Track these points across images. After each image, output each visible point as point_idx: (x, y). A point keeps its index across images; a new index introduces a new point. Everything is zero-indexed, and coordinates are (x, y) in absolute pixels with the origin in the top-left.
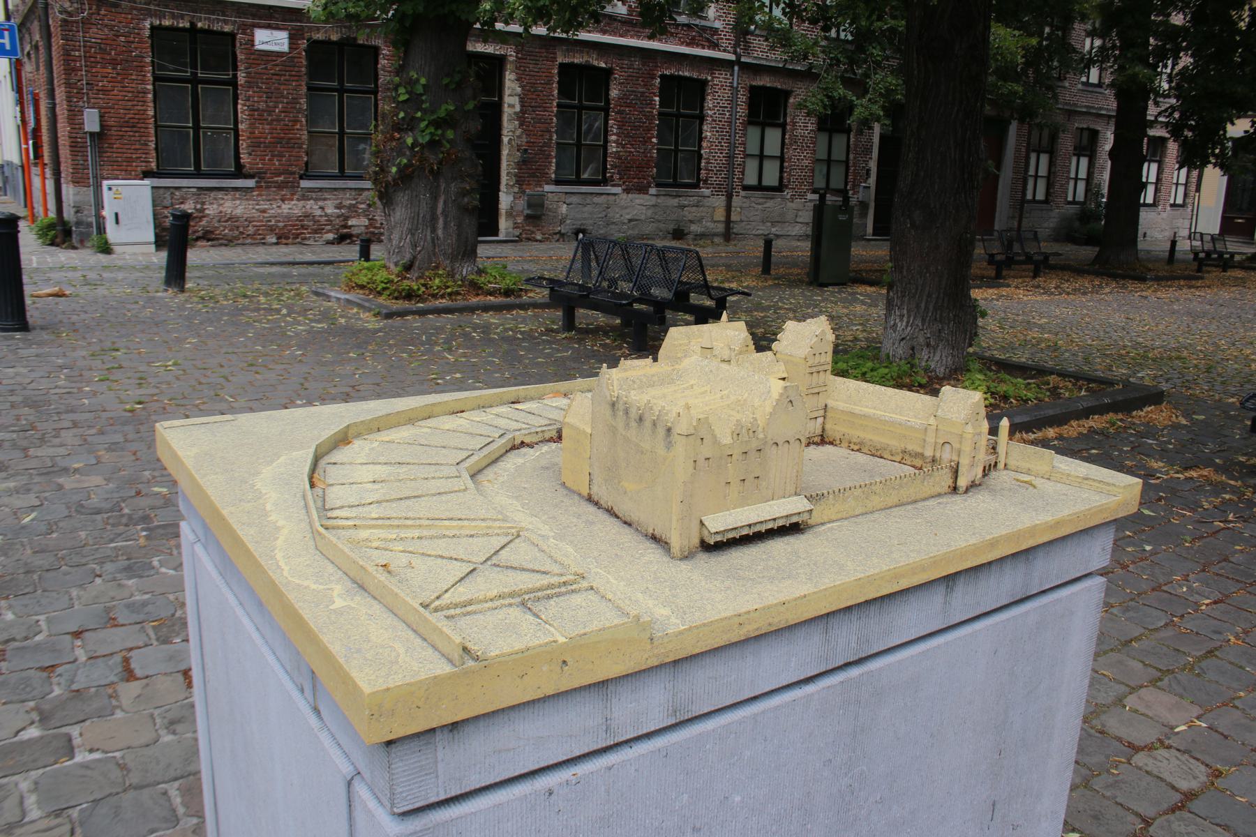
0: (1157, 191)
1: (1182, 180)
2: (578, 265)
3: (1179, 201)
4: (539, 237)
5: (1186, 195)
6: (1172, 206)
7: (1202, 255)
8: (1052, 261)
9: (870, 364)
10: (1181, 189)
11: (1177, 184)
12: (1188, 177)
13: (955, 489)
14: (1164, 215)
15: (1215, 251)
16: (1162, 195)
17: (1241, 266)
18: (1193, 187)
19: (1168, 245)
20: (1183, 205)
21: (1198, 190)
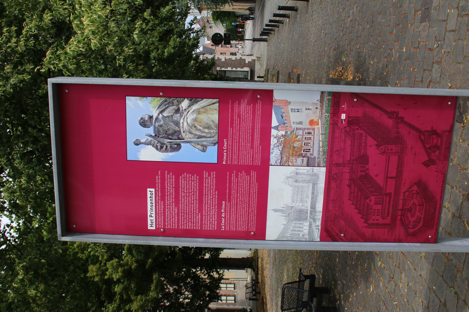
0: (229, 296)
1: (225, 286)
2: (193, 144)
3: (233, 286)
4: (459, 19)
5: (230, 284)
6: (235, 289)
7: (254, 293)
8: (254, 278)
9: (357, 127)
10: (228, 286)
11: (226, 288)
12: (223, 284)
13: (387, 177)
14: (238, 292)
15: (252, 287)
16: (230, 293)
17: (257, 274)
18: (227, 281)
19: (251, 301)
20: (235, 296)
21: (228, 279)
